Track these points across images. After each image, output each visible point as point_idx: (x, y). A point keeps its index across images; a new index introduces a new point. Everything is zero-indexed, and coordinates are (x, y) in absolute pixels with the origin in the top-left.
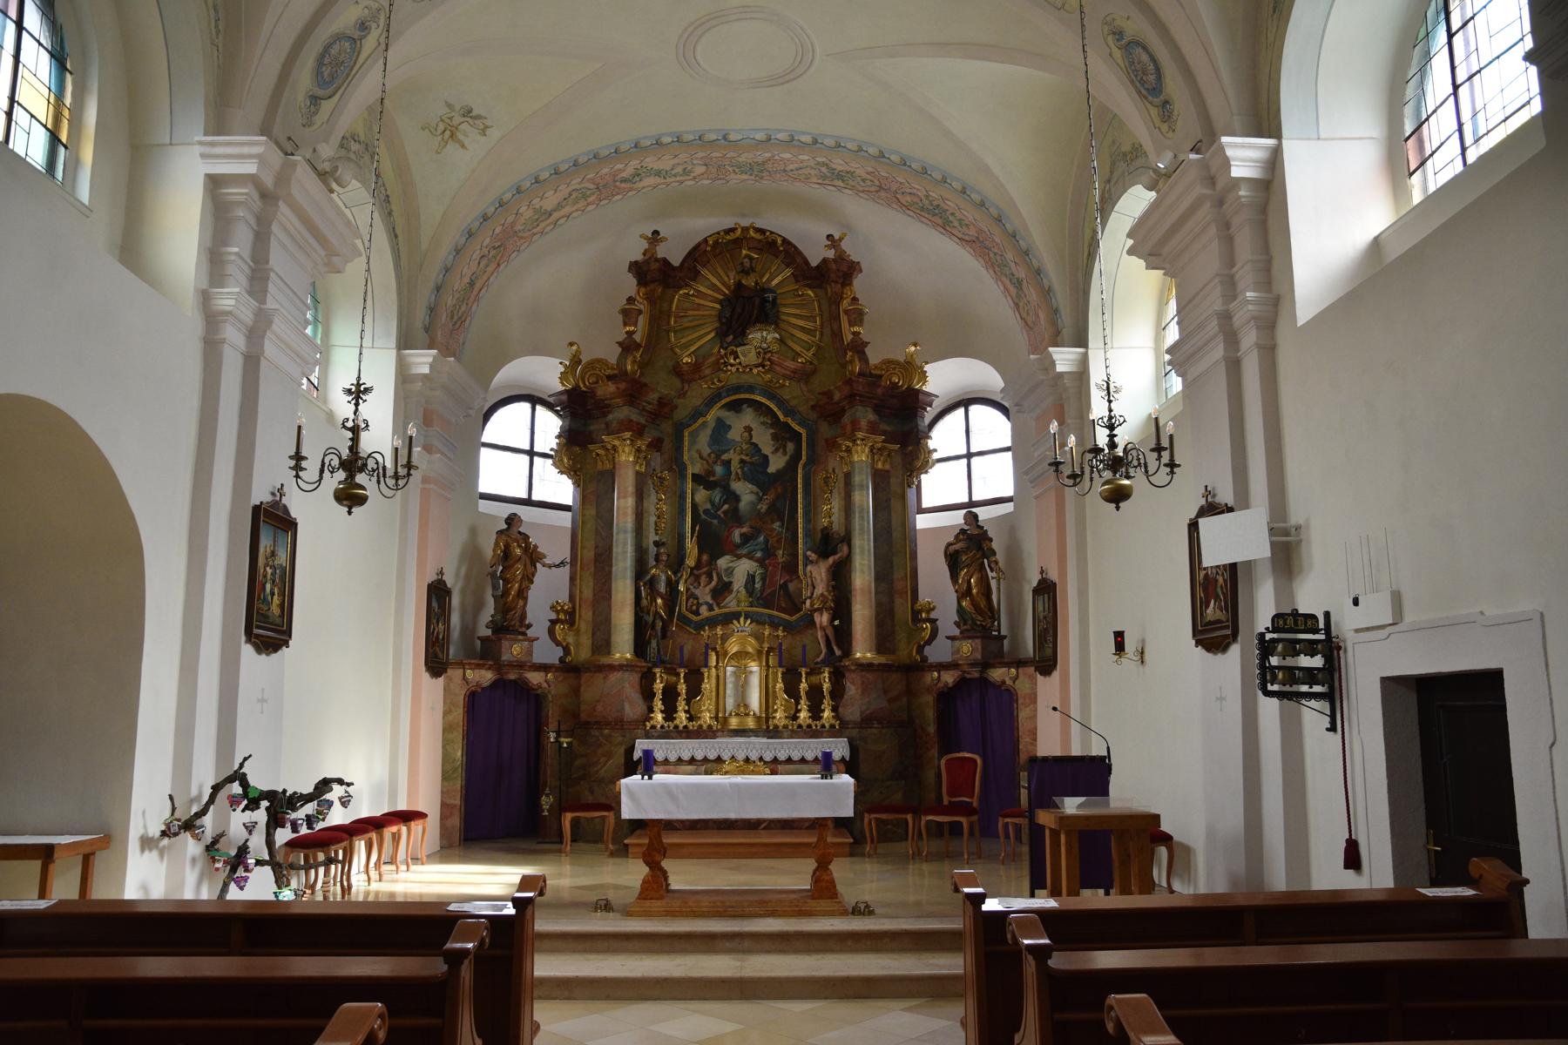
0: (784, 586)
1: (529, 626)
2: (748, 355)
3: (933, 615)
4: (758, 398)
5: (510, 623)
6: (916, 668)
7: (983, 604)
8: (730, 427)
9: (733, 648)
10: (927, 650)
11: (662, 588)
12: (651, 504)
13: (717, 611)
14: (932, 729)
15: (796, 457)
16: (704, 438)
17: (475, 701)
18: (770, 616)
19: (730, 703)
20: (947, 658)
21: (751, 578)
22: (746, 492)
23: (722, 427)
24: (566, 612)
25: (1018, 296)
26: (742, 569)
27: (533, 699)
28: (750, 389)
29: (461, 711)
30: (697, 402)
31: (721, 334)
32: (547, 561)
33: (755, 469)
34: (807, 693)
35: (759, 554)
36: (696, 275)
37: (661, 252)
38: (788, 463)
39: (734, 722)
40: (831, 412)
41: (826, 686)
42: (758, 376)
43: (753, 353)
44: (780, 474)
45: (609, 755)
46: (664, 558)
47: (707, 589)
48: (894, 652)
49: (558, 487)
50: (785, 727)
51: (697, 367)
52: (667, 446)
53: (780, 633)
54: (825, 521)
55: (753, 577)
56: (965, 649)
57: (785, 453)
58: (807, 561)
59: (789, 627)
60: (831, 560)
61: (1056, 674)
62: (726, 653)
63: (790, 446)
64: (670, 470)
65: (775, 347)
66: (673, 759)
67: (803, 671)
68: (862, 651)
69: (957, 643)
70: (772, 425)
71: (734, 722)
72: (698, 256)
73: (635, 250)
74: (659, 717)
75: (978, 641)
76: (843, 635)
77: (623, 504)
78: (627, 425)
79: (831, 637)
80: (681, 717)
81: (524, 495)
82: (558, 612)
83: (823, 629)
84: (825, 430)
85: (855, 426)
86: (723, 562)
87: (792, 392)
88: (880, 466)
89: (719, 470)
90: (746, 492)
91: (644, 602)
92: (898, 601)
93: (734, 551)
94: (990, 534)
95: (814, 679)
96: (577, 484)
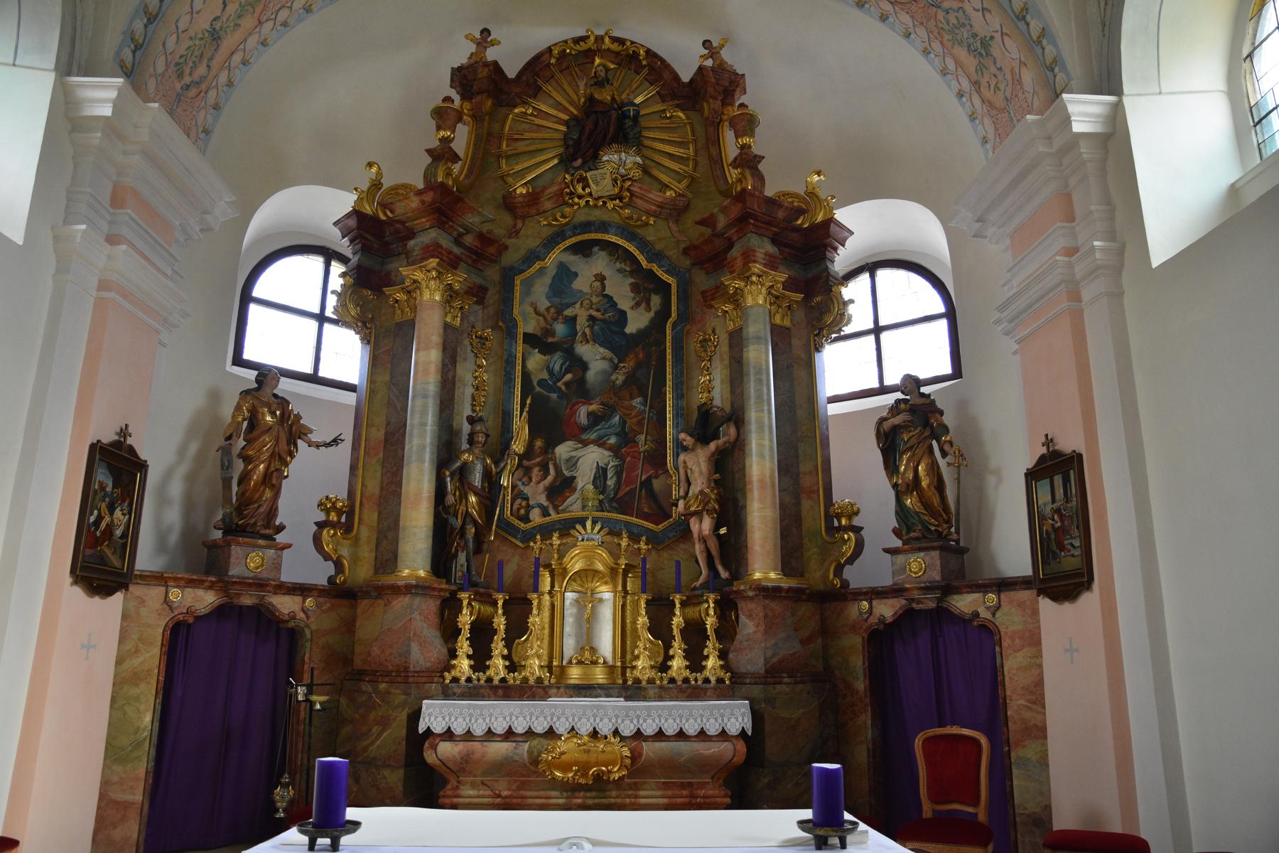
0: (647, 484)
1: (281, 528)
2: (601, 181)
3: (856, 522)
4: (614, 239)
5: (249, 517)
6: (837, 595)
7: (936, 501)
8: (576, 274)
9: (575, 564)
10: (848, 572)
11: (477, 479)
12: (465, 372)
13: (554, 516)
14: (861, 685)
15: (664, 314)
16: (540, 293)
17: (180, 636)
18: (627, 524)
19: (570, 646)
20: (887, 581)
21: (601, 473)
22: (596, 358)
23: (565, 274)
24: (339, 512)
25: (981, 68)
26: (588, 460)
27: (286, 637)
28: (604, 227)
29: (156, 651)
30: (533, 243)
31: (566, 161)
32: (314, 438)
33: (609, 328)
34: (682, 632)
35: (613, 440)
36: (536, 92)
37: (491, 54)
38: (652, 321)
39: (575, 674)
40: (713, 256)
41: (711, 622)
42: (612, 212)
43: (608, 181)
44: (642, 335)
45: (384, 723)
46: (481, 438)
47: (541, 486)
48: (802, 575)
49: (346, 355)
50: (651, 681)
51: (534, 198)
52: (492, 297)
53: (643, 546)
54: (703, 398)
55: (605, 470)
56: (914, 567)
57: (648, 309)
58: (681, 448)
59: (653, 539)
60: (713, 446)
61: (1089, 601)
62: (565, 571)
63: (656, 300)
64: (495, 327)
65: (636, 173)
66: (479, 731)
67: (677, 599)
68: (763, 568)
69: (900, 559)
70: (632, 274)
71: (575, 674)
72: (539, 69)
73: (461, 53)
74: (464, 665)
75: (936, 554)
76: (732, 548)
77: (424, 361)
78: (433, 250)
79: (714, 552)
80: (498, 666)
81: (308, 369)
82: (328, 512)
83: (703, 540)
84: (702, 281)
85: (748, 257)
86: (563, 450)
87: (658, 232)
88: (778, 320)
89: (560, 329)
90: (596, 358)
91: (450, 499)
92: (806, 504)
93: (578, 435)
94: (939, 405)
95: (692, 612)
96: (366, 340)
